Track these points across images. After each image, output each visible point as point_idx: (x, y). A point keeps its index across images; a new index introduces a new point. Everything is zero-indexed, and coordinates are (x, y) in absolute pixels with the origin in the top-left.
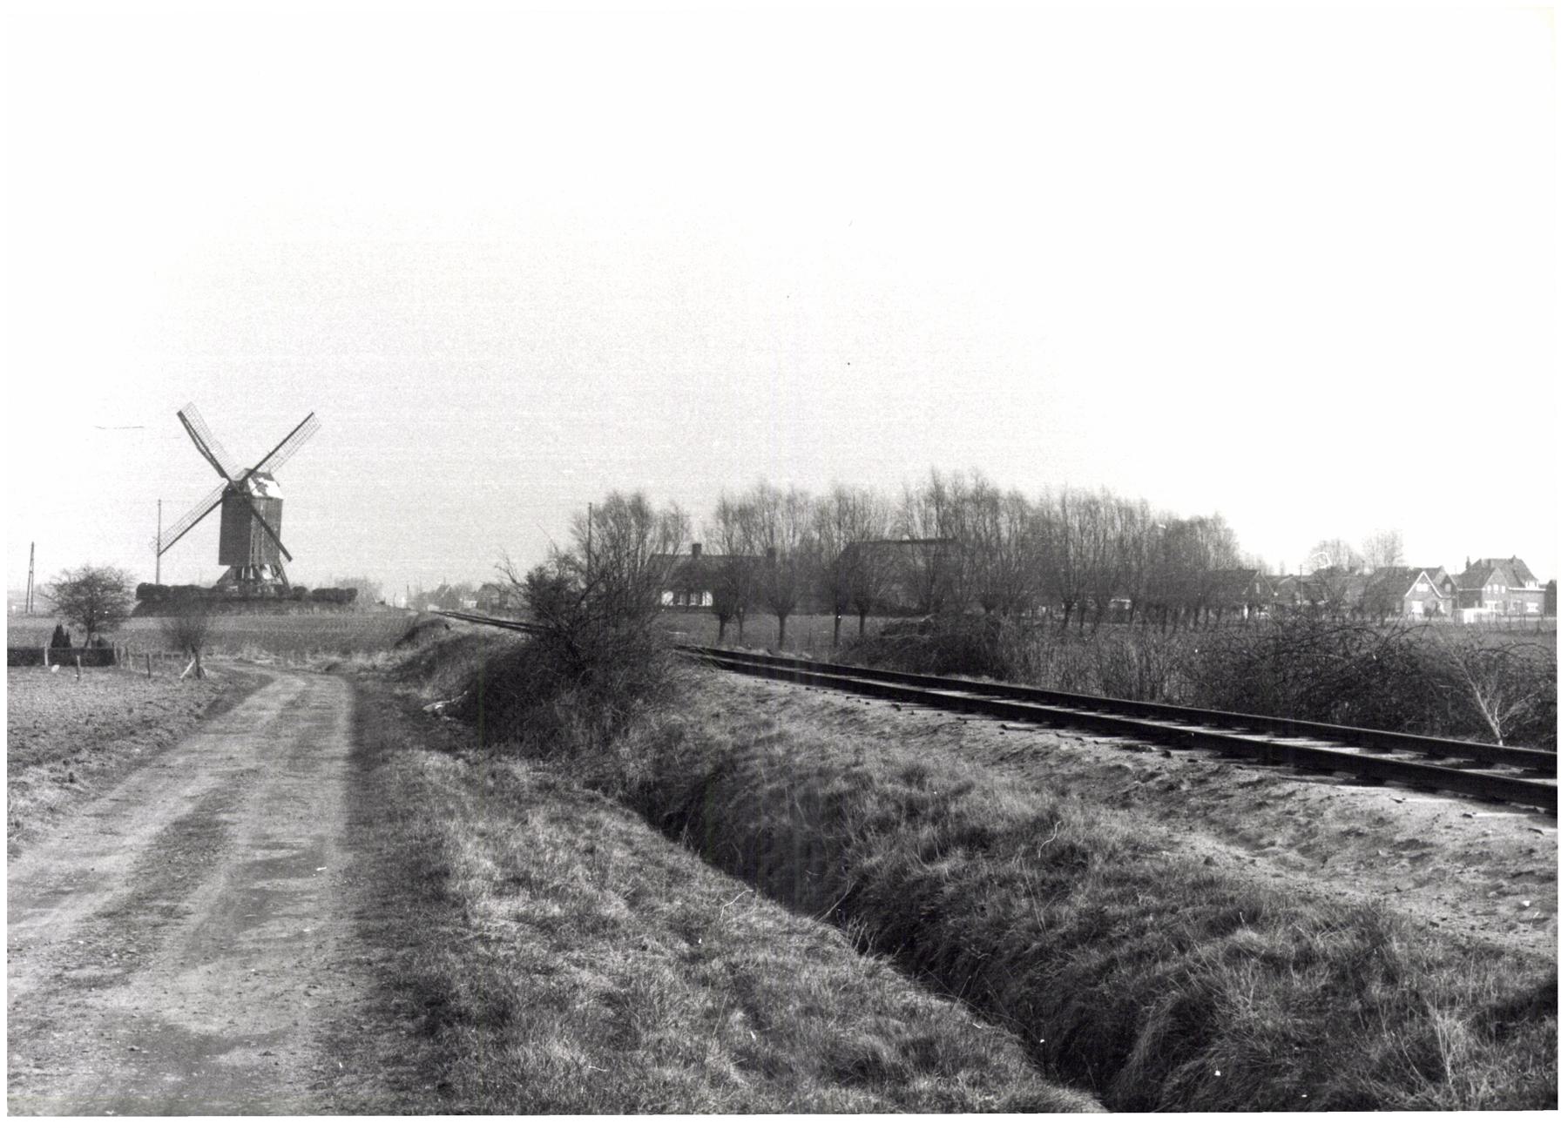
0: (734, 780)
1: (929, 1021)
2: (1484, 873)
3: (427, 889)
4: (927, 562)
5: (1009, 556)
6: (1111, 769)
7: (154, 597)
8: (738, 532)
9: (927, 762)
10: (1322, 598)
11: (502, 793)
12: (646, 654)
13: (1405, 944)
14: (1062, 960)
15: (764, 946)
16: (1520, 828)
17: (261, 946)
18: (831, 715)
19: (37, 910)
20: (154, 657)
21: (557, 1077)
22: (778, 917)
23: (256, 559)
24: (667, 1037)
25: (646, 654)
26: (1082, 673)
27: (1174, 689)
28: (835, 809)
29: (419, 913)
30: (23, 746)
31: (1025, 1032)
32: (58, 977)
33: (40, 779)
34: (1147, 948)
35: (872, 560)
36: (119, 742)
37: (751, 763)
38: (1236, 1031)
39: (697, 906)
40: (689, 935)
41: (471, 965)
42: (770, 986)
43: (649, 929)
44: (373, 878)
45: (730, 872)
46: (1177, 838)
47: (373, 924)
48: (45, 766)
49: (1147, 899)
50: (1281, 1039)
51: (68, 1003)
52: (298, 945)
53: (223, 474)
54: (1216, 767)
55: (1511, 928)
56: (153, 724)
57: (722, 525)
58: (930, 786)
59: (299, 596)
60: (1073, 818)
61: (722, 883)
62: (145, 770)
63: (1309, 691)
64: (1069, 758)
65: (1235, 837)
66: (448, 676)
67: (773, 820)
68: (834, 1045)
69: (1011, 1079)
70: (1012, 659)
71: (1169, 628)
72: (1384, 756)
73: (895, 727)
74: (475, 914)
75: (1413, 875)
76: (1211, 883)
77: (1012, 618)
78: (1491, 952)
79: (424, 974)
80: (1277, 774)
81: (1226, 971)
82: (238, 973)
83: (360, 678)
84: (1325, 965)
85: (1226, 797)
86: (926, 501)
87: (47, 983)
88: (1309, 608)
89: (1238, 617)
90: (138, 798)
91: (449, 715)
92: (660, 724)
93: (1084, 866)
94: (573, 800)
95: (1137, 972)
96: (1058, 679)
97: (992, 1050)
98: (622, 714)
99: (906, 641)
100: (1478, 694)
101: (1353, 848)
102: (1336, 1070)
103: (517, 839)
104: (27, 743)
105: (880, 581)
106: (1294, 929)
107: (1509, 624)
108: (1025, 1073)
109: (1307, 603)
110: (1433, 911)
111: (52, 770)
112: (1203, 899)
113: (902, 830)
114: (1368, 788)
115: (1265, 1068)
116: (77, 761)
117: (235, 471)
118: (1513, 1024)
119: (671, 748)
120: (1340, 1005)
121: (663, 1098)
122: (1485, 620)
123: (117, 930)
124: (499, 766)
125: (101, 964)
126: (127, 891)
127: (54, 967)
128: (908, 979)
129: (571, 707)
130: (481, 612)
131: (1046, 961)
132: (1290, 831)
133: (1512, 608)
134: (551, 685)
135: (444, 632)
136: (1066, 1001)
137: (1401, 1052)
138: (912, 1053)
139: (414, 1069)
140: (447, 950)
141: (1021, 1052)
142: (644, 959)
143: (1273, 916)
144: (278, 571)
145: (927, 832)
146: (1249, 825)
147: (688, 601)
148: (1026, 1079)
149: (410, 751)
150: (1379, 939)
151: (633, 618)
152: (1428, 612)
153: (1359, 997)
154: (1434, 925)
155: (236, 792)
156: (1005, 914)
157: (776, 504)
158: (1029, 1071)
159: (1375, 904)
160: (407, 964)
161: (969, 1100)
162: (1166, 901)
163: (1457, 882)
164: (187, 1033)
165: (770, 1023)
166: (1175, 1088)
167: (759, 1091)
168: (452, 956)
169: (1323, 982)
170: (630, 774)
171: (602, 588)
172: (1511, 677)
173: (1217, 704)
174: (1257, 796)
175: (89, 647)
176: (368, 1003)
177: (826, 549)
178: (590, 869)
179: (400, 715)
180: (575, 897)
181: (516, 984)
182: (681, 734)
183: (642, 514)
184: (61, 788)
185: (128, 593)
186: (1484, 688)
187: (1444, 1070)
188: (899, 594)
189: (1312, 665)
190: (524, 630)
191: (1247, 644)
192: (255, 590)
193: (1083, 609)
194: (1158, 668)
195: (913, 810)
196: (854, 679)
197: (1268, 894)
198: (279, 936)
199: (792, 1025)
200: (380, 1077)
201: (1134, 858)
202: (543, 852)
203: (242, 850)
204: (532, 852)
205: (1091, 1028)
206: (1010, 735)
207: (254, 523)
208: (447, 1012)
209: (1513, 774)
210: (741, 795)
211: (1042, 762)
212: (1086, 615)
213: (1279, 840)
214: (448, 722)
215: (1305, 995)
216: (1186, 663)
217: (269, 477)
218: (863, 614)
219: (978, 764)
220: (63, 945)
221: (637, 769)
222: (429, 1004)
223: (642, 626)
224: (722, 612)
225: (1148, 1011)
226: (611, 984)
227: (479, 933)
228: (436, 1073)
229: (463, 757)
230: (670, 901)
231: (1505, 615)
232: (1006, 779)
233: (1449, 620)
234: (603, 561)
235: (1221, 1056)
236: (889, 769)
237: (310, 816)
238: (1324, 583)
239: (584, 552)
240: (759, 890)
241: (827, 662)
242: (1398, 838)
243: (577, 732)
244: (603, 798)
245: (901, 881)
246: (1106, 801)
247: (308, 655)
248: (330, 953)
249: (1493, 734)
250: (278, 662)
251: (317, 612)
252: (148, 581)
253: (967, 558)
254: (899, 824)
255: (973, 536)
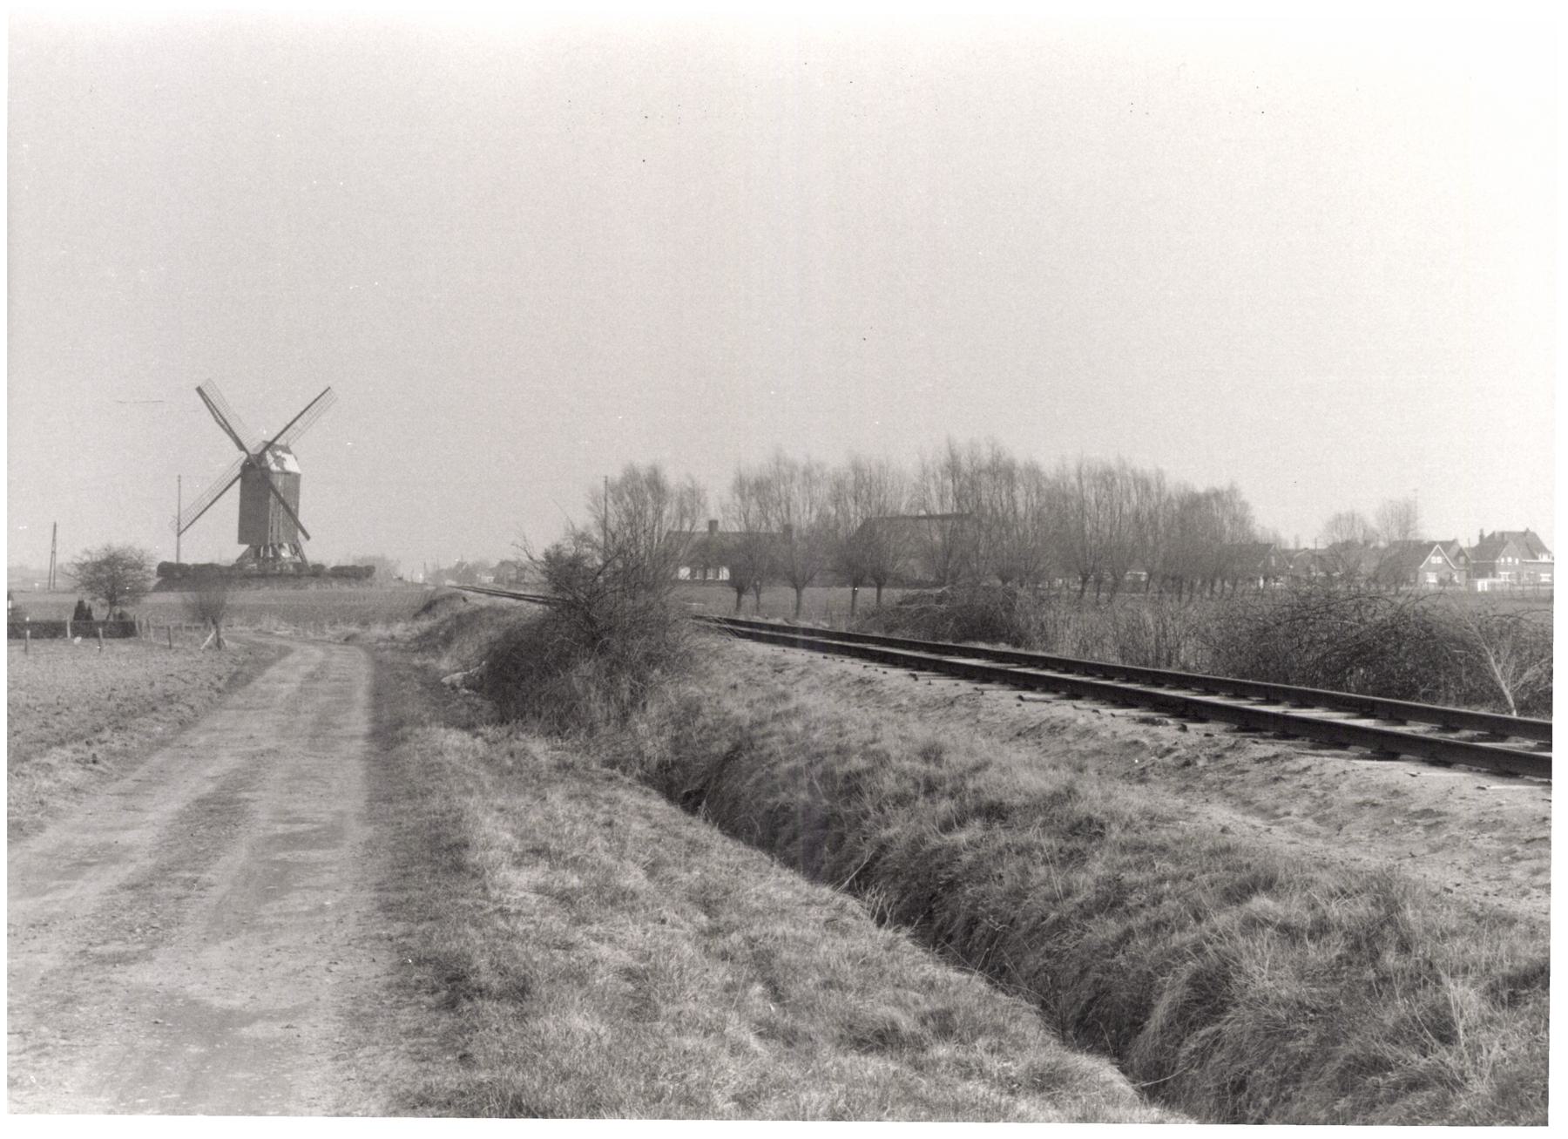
0: (752, 758)
1: (947, 994)
2: (1499, 839)
3: (446, 861)
4: (944, 538)
5: (1026, 531)
6: (1127, 745)
7: (173, 575)
8: (755, 509)
9: (944, 738)
10: (1337, 570)
11: (521, 772)
12: (663, 624)
13: (1419, 912)
14: (1079, 931)
15: (782, 919)
16: (1534, 799)
17: (282, 920)
18: (848, 685)
19: (61, 882)
20: (176, 628)
21: (577, 1047)
22: (797, 887)
23: (275, 538)
24: (687, 1009)
25: (663, 624)
26: (1098, 640)
27: (1192, 657)
28: (852, 786)
29: (439, 884)
30: (46, 725)
31: (1043, 1002)
32: (83, 952)
33: (64, 760)
34: (1163, 918)
35: (888, 535)
36: (141, 720)
37: (769, 740)
38: (1251, 1000)
39: (715, 877)
40: (708, 907)
41: (491, 941)
42: (789, 960)
43: (668, 901)
44: (393, 850)
45: (749, 842)
46: (1194, 809)
47: (394, 897)
48: (68, 747)
49: (1165, 866)
50: (1296, 1006)
51: (93, 979)
52: (318, 919)
53: (241, 446)
54: (1232, 742)
55: (1524, 894)
56: (174, 698)
57: (738, 500)
58: (948, 763)
59: (317, 572)
60: (1091, 792)
61: (740, 853)
62: (167, 751)
63: (1325, 656)
64: (1086, 732)
65: (1251, 808)
66: (466, 646)
67: (791, 796)
68: (853, 1015)
69: (1029, 1046)
70: (1029, 626)
71: (1185, 597)
72: (1400, 729)
73: (913, 699)
74: (494, 885)
75: (1427, 841)
76: (1228, 850)
77: (1028, 589)
78: (1505, 919)
79: (445, 950)
80: (1293, 749)
81: (1242, 942)
82: (260, 948)
83: (378, 649)
84: (1340, 934)
85: (1243, 772)
86: (942, 472)
87: (72, 959)
88: (1323, 579)
89: (1254, 587)
90: (160, 778)
91: (467, 688)
92: (678, 697)
93: (1102, 835)
94: (592, 779)
95: (1154, 942)
96: (1075, 646)
97: (1010, 1019)
98: (640, 685)
99: (923, 610)
100: (1492, 660)
101: (1368, 815)
102: (1350, 1034)
103: (536, 814)
104: (50, 721)
105: (896, 557)
106: (1309, 896)
107: (1522, 593)
108: (1043, 1039)
109: (1322, 574)
110: (1448, 876)
111: (75, 751)
112: (1220, 865)
113: (920, 804)
114: (1383, 763)
115: (1281, 1033)
116: (100, 742)
117: (253, 444)
118: (1526, 991)
119: (689, 724)
120: (1355, 974)
121: (683, 1066)
122: (1498, 588)
123: (140, 903)
124: (517, 745)
125: (124, 939)
126: (150, 862)
127: (79, 943)
128: (927, 952)
129: (588, 678)
130: (499, 586)
131: (1064, 932)
132: (1306, 801)
133: (1525, 578)
134: (568, 655)
135: (462, 604)
136: (1083, 972)
137: (1414, 1018)
138: (931, 1022)
139: (435, 1040)
140: (467, 924)
141: (1039, 1021)
142: (663, 933)
143: (1289, 882)
144: (296, 549)
145: (945, 806)
146: (1265, 797)
147: (705, 575)
148: (1044, 1046)
149: (428, 729)
150: (1393, 907)
151: (651, 590)
152: (1441, 582)
153: (1373, 966)
154: (1448, 891)
155: (257, 772)
156: (1022, 883)
157: (792, 478)
158: (1048, 1038)
159: (1390, 869)
160: (427, 939)
161: (987, 1067)
162: (1183, 868)
163: (1471, 847)
164: (209, 1008)
165: (789, 996)
166: (1191, 1053)
167: (779, 1059)
168: (472, 931)
169: (1338, 952)
170: (647, 753)
171: (619, 564)
172: (1526, 642)
173: (1233, 671)
174: (1273, 771)
175: (111, 619)
176: (388, 979)
177: (843, 525)
178: (609, 840)
179: (419, 688)
180: (593, 868)
181: (535, 959)
182: (699, 708)
183: (658, 488)
184: (84, 769)
185: (149, 571)
186: (1497, 653)
187: (1456, 1033)
188: (916, 568)
189: (1328, 631)
190: (541, 603)
191: (1263, 612)
192: (275, 568)
193: (1099, 581)
194: (1175, 635)
195: (931, 787)
196: (872, 647)
197: (1283, 861)
198: (300, 909)
199: (810, 998)
200: (402, 1048)
201: (1151, 828)
202: (562, 825)
203: (264, 825)
204: (550, 825)
205: (1109, 998)
206: (1027, 706)
207: (272, 500)
208: (468, 988)
209: (1527, 748)
210: (759, 774)
211: (1059, 738)
212: (1102, 586)
213: (1295, 811)
214: (466, 695)
215: (1319, 965)
216: (1202, 629)
217: (287, 450)
218: (880, 586)
219: (996, 740)
220: (87, 920)
221: (655, 748)
222: (449, 980)
223: (659, 598)
224: (739, 586)
225: (1164, 982)
226: (631, 959)
227: (499, 906)
228: (457, 1045)
229: (482, 735)
230: (689, 871)
231: (1519, 584)
232: (1024, 756)
233: (1463, 589)
234: (619, 538)
235: (1238, 1022)
236: (906, 746)
237: (330, 794)
238: (1339, 555)
239: (600, 530)
240: (777, 859)
241: (844, 631)
242: (1413, 808)
243: (594, 706)
244: (622, 777)
245: (919, 850)
246: (1123, 777)
247: (327, 626)
248: (351, 929)
249: (1507, 703)
250: (297, 633)
251: (336, 587)
252: (168, 560)
253: (983, 533)
254: (917, 799)
255: (989, 511)
